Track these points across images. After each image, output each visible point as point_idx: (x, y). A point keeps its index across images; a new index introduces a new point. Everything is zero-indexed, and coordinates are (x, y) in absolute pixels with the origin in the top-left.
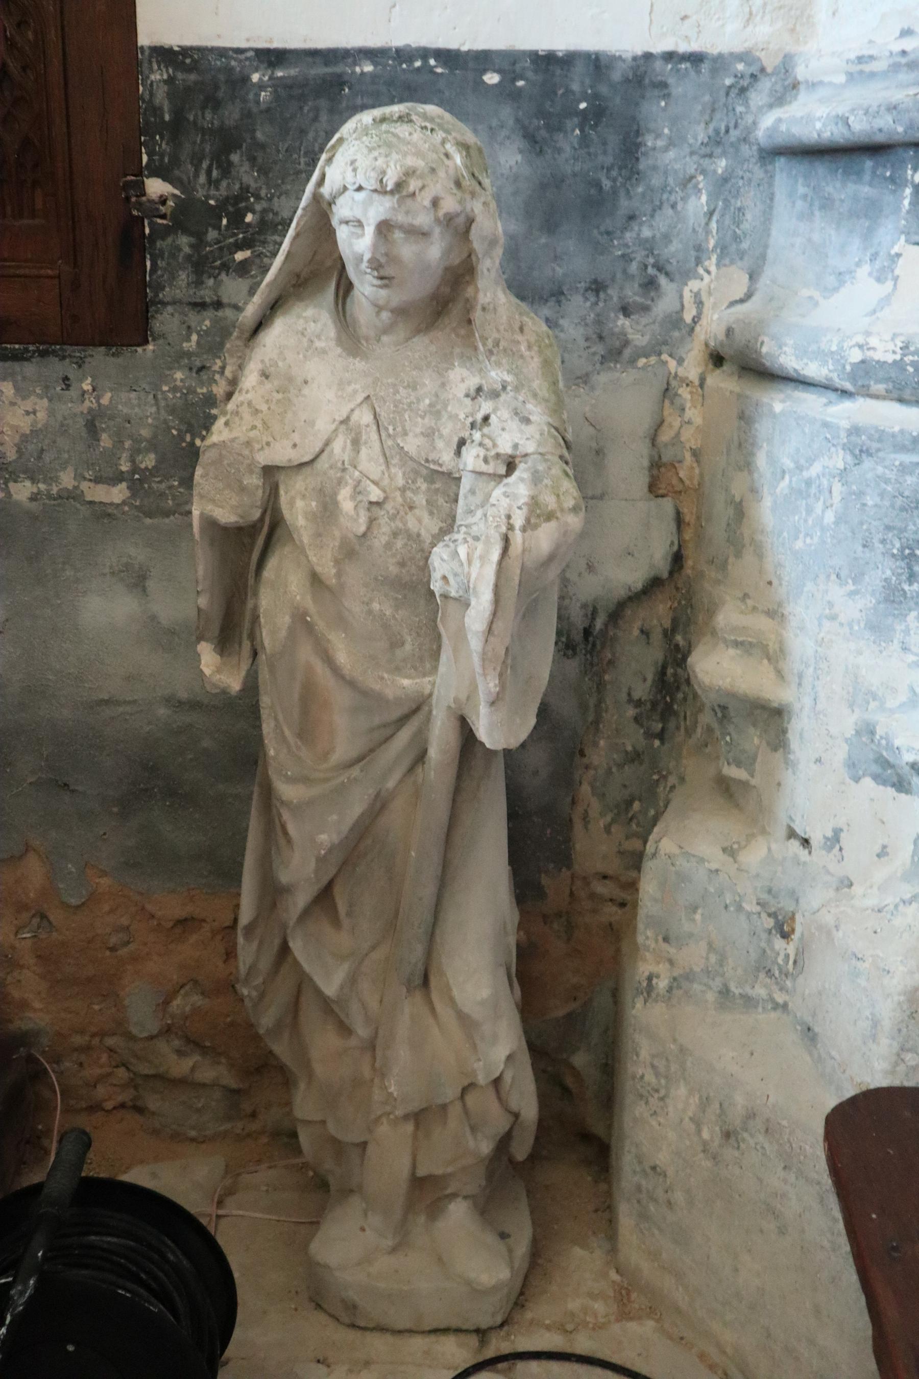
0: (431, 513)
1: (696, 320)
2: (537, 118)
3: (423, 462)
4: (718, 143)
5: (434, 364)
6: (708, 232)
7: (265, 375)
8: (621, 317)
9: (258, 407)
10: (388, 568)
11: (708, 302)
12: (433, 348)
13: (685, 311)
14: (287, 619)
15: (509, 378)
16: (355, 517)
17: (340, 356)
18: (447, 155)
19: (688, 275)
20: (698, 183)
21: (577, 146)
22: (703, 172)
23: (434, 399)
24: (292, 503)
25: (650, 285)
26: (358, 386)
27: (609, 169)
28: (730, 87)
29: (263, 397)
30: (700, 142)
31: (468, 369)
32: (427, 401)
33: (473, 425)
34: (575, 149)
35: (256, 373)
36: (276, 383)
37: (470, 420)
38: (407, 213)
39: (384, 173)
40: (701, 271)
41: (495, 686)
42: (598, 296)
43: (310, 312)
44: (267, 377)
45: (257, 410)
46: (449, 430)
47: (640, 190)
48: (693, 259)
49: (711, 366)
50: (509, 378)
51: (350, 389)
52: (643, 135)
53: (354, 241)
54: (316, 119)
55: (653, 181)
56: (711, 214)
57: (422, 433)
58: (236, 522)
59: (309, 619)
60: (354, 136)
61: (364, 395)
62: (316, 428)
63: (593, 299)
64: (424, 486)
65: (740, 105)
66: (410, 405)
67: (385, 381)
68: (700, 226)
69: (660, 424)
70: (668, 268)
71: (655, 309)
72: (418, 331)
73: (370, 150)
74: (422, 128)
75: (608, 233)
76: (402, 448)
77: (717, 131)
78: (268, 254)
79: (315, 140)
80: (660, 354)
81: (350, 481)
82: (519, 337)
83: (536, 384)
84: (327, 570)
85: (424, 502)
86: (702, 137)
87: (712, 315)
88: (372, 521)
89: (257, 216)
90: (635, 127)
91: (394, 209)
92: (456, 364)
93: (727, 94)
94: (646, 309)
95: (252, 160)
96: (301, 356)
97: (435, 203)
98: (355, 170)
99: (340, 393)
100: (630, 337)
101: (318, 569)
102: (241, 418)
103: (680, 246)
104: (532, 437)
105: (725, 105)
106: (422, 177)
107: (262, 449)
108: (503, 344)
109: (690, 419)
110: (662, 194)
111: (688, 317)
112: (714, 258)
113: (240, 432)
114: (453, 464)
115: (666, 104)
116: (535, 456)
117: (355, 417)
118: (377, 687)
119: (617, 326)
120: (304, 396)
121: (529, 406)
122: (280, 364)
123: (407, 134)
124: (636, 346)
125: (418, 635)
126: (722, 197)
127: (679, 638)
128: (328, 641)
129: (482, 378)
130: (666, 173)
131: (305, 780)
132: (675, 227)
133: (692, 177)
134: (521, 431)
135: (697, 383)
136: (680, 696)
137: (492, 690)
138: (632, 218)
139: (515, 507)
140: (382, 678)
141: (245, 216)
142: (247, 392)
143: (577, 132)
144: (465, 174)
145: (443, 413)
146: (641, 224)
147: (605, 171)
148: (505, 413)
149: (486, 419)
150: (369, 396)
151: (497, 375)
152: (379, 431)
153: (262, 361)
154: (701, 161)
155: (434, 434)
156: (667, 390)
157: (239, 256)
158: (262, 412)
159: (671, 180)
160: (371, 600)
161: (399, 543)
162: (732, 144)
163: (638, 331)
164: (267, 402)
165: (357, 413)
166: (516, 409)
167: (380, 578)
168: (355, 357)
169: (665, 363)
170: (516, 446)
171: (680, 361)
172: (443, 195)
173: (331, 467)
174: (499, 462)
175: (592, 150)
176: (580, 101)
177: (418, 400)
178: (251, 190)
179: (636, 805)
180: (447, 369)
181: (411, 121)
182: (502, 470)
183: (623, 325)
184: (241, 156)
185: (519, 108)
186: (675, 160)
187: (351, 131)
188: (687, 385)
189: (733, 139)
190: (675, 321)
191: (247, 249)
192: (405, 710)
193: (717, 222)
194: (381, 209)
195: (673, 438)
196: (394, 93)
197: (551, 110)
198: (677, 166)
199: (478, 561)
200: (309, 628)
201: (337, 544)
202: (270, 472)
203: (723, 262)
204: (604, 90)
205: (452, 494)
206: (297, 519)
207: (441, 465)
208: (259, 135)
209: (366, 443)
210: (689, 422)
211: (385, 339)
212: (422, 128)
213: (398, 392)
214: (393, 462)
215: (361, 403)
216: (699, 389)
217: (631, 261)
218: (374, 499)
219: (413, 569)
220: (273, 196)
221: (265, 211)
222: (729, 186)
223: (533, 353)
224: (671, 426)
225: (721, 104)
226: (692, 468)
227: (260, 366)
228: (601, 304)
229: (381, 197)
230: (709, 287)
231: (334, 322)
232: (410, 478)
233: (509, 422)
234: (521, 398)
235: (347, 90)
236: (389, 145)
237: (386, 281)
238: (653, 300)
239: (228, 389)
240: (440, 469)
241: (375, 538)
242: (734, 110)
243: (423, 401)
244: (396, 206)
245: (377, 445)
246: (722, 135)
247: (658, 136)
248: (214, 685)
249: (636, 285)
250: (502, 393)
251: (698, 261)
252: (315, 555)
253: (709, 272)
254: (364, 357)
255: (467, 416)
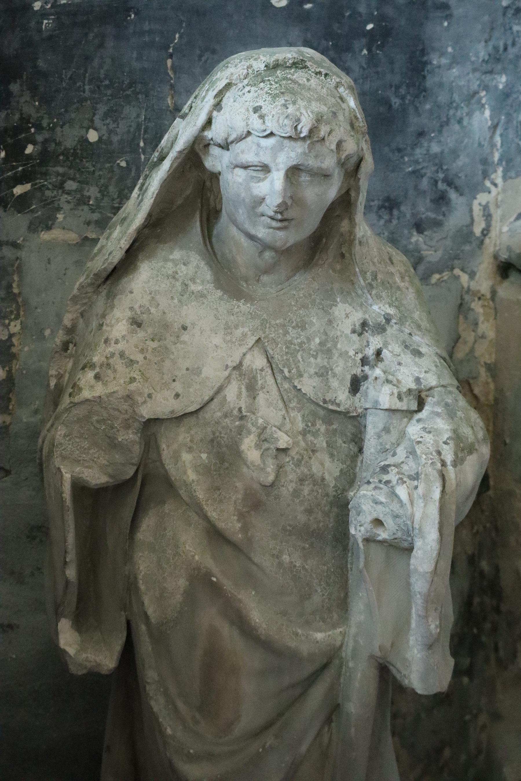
0: (332, 456)
1: (486, 232)
2: (326, 39)
3: (321, 404)
4: (498, 60)
5: (318, 301)
6: (493, 146)
7: (137, 323)
8: (415, 233)
9: (132, 357)
10: (296, 517)
11: (497, 214)
12: (315, 285)
13: (475, 224)
14: (183, 582)
15: (391, 311)
16: (262, 466)
17: (221, 299)
18: (341, 98)
19: (475, 188)
20: (481, 98)
21: (365, 66)
22: (486, 88)
23: (324, 337)
24: (176, 457)
25: (441, 200)
26: (246, 330)
27: (398, 87)
28: (506, 8)
29: (136, 346)
30: (481, 60)
31: (350, 305)
32: (317, 340)
33: (364, 361)
34: (364, 69)
35: (124, 322)
36: (150, 330)
37: (360, 356)
38: (316, 157)
39: (298, 120)
40: (488, 184)
41: (437, 627)
42: (391, 214)
43: (177, 254)
44: (139, 325)
45: (131, 361)
46: (343, 369)
47: (428, 107)
48: (480, 172)
49: (499, 279)
50: (391, 311)
51: (238, 332)
52: (428, 54)
53: (252, 184)
54: (101, 45)
55: (440, 98)
56: (494, 127)
57: (316, 373)
58: (107, 482)
59: (214, 579)
60: (246, 82)
61: (255, 338)
62: (203, 375)
63: (386, 217)
64: (323, 428)
65: (516, 24)
66: (301, 344)
67: (273, 322)
68: (485, 139)
69: (457, 339)
70: (457, 182)
71: (447, 224)
72: (296, 270)
73: (275, 97)
74: (316, 74)
75: (399, 150)
76: (300, 390)
77: (496, 49)
78: (50, 186)
79: (101, 66)
80: (452, 269)
81: (253, 429)
82: (392, 269)
83: (417, 315)
84: (230, 524)
85: (325, 444)
86: (483, 54)
87: (501, 226)
88: (280, 467)
89: (39, 147)
90: (420, 47)
91: (305, 153)
92: (338, 300)
93: (504, 14)
94: (438, 224)
95: (33, 89)
96: (176, 301)
97: (339, 144)
98: (262, 117)
99: (228, 338)
100: (424, 253)
101: (221, 525)
102: (115, 371)
103: (467, 160)
104: (430, 370)
105: (503, 25)
106: (328, 123)
107: (145, 402)
108: (379, 276)
109: (484, 333)
110: (448, 110)
111: (477, 230)
112: (500, 170)
113: (116, 385)
114: (349, 402)
115: (449, 23)
116: (439, 389)
117: (247, 362)
118: (292, 644)
119: (411, 243)
120: (184, 343)
121: (417, 338)
122: (153, 310)
123: (305, 80)
124: (429, 262)
125: (328, 584)
126: (504, 111)
127: (484, 565)
128: (240, 601)
129: (365, 312)
130: (451, 91)
131: (210, 757)
132: (462, 142)
133: (476, 93)
134: (416, 364)
135: (488, 296)
136: (488, 626)
137: (434, 632)
138: (421, 134)
139: (441, 443)
140: (297, 634)
141: (25, 147)
142: (117, 342)
143: (365, 52)
144: (359, 116)
145: (334, 351)
146: (431, 140)
147: (393, 89)
148: (397, 348)
149: (378, 353)
150: (260, 338)
151: (379, 309)
152: (274, 374)
153: (131, 308)
154: (483, 77)
155: (327, 372)
156: (461, 305)
157: (18, 190)
158: (138, 362)
159: (456, 97)
160: (281, 552)
161: (306, 490)
162: (511, 61)
163: (431, 247)
164: (142, 351)
165: (248, 357)
166: (404, 342)
167: (288, 528)
168: (238, 300)
169: (458, 278)
170: (418, 380)
171: (472, 275)
172: (346, 138)
173: (226, 416)
174: (411, 397)
175: (379, 69)
176: (368, 23)
177: (309, 339)
178: (31, 120)
179: (447, 753)
180: (331, 306)
181: (305, 67)
182: (414, 407)
183: (418, 240)
184: (21, 85)
185: (307, 30)
186: (459, 77)
187: (242, 77)
188: (479, 299)
189: (511, 56)
190: (465, 235)
191: (27, 183)
192: (316, 666)
193: (501, 135)
194: (293, 155)
195: (467, 354)
196: (182, 18)
197: (339, 31)
198: (462, 83)
199: (421, 501)
200: (216, 589)
201: (240, 496)
202: (151, 427)
203: (509, 174)
204: (389, 11)
205: (349, 434)
206: (185, 473)
207: (338, 405)
208: (41, 63)
209: (262, 388)
210: (483, 337)
211: (265, 278)
212: (316, 74)
213: (289, 333)
214: (291, 405)
215: (253, 346)
216: (491, 303)
217: (422, 176)
218: (282, 445)
219: (320, 516)
220: (55, 125)
221: (46, 141)
222: (510, 101)
223: (407, 284)
224: (465, 342)
225: (499, 23)
226: (487, 383)
227: (129, 314)
228: (395, 222)
229: (293, 143)
230: (497, 199)
231: (207, 264)
232: (309, 421)
233: (402, 355)
234: (407, 331)
235: (133, 16)
236: (293, 92)
237: (286, 223)
238: (444, 215)
239: (66, 338)
240: (338, 409)
241: (283, 486)
242: (511, 28)
243: (314, 339)
244: (307, 152)
245: (274, 388)
246: (501, 52)
247: (443, 54)
248: (80, 665)
249: (428, 201)
250: (387, 326)
251: (485, 175)
252: (214, 510)
253: (496, 185)
254: (249, 298)
255: (357, 353)
